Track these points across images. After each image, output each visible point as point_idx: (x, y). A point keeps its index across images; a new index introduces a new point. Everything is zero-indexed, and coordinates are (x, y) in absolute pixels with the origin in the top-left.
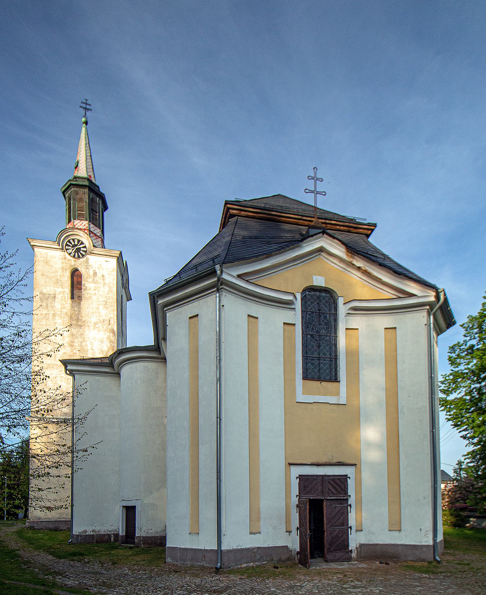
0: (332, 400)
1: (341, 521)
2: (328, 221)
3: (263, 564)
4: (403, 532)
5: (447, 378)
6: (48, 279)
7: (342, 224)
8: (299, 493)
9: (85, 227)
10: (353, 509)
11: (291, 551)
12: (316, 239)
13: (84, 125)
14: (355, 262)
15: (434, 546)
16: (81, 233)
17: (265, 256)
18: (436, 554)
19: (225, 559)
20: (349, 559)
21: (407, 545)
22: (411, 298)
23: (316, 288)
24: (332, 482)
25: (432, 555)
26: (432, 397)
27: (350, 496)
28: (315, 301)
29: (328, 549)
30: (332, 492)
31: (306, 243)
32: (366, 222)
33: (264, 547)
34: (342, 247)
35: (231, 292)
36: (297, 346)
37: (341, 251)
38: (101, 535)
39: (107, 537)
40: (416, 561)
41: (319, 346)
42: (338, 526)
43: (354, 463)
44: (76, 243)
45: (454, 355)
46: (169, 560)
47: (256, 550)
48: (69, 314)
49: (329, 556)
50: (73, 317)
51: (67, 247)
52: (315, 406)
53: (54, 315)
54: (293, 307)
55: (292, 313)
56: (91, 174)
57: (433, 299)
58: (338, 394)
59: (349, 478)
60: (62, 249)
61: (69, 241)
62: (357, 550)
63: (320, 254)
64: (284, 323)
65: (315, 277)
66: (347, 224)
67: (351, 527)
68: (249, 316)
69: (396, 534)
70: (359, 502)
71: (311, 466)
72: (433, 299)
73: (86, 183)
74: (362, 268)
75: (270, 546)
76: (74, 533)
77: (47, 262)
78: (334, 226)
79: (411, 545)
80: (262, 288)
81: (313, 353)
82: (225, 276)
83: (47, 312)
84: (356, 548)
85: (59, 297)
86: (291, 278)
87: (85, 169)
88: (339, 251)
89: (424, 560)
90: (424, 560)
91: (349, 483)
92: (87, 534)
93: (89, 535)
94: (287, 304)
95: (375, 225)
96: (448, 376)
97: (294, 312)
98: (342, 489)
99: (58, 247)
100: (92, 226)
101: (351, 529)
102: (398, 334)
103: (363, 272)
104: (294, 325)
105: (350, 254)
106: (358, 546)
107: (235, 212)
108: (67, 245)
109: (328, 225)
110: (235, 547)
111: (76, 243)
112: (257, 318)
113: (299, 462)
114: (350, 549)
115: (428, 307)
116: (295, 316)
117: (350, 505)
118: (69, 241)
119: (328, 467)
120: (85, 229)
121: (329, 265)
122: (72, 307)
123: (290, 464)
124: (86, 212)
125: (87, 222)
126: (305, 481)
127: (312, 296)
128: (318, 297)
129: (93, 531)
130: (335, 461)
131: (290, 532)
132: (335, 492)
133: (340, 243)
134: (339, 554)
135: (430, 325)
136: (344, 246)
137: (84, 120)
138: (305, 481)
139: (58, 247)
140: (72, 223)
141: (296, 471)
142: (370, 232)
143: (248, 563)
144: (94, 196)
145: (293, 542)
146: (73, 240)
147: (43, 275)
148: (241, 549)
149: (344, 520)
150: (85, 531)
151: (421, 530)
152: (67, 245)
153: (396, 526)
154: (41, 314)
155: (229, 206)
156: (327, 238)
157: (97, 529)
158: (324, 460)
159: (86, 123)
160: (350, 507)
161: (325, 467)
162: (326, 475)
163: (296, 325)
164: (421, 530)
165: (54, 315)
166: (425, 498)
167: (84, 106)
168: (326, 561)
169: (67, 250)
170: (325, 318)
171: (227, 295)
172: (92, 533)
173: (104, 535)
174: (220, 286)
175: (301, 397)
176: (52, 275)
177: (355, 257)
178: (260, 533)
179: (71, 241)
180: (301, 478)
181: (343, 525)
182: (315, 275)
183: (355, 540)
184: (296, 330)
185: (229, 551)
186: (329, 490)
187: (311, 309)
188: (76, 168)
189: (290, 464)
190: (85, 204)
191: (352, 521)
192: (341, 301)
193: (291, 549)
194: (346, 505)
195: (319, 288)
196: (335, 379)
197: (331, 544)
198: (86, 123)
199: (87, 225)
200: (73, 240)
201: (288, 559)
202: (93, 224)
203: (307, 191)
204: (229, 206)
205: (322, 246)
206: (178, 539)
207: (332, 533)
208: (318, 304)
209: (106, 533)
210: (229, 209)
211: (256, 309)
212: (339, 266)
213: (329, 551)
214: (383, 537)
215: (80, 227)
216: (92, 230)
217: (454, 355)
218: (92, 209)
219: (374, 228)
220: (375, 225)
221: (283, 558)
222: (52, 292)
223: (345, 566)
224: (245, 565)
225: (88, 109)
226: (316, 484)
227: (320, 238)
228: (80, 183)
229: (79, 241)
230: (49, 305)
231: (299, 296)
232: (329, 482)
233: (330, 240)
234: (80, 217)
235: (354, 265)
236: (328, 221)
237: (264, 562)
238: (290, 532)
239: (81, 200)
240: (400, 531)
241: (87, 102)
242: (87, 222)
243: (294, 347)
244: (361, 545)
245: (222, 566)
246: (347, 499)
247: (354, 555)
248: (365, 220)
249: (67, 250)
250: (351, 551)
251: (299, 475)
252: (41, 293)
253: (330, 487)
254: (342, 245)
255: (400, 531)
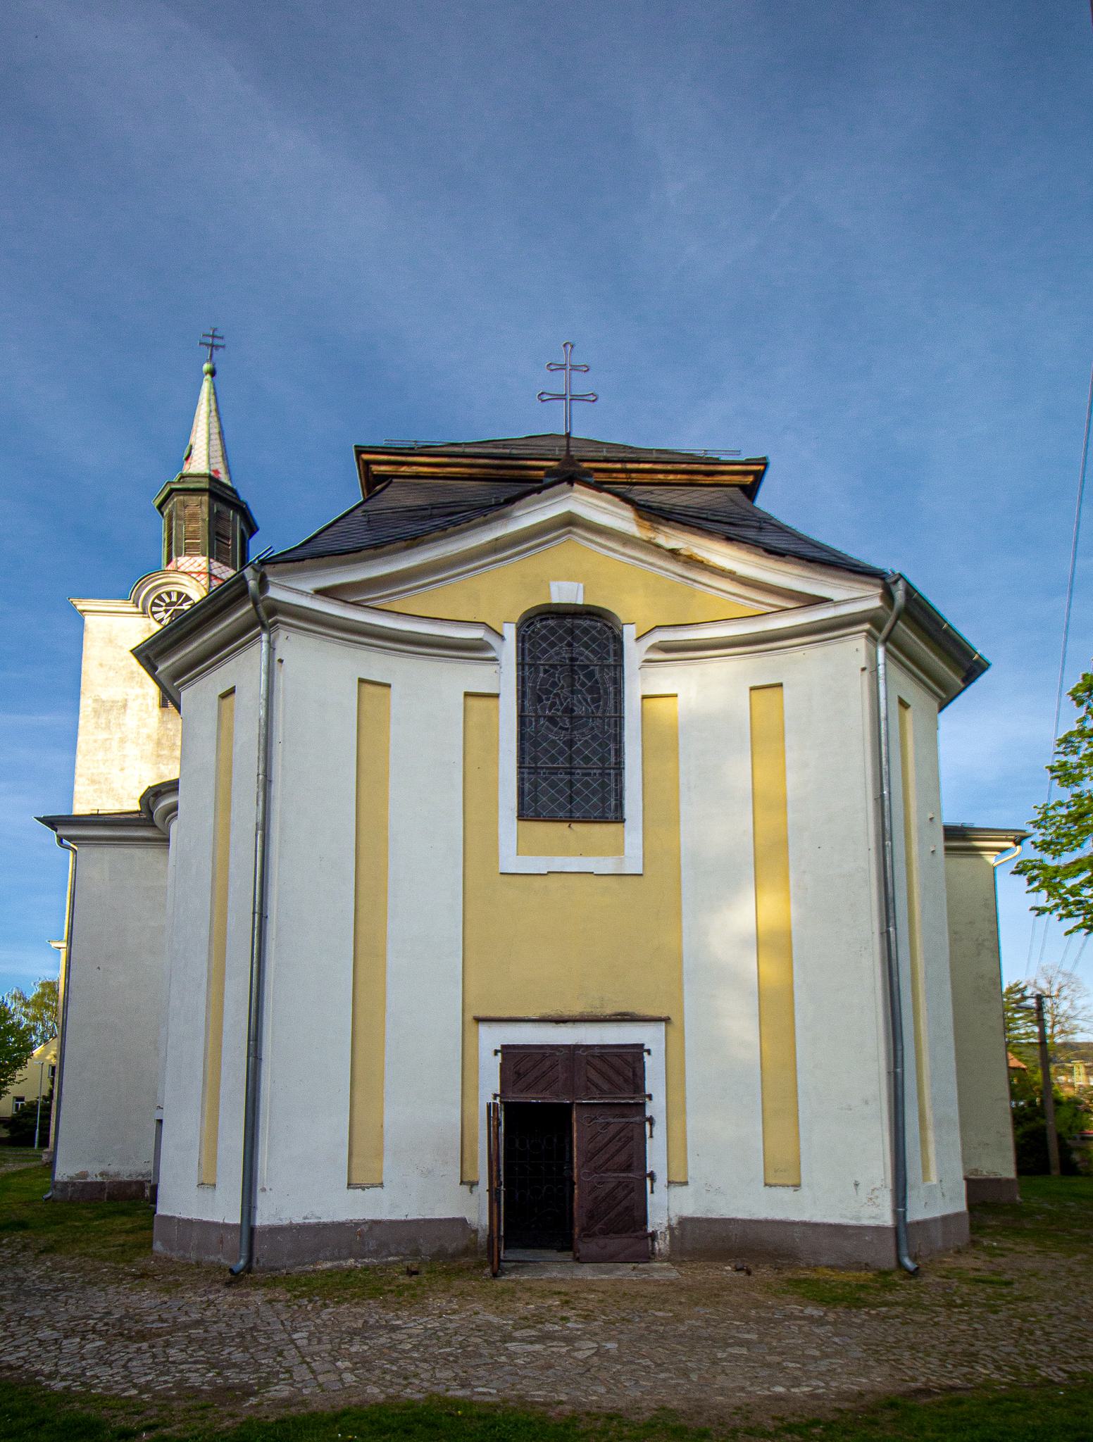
0: (605, 865)
1: (622, 1158)
2: (629, 466)
3: (388, 1264)
4: (805, 1190)
5: (1051, 813)
6: (111, 674)
7: (669, 467)
8: (502, 1091)
9: (200, 569)
10: (659, 1130)
11: (476, 1231)
12: (547, 499)
13: (208, 377)
14: (661, 540)
15: (896, 1230)
16: (184, 579)
17: (403, 544)
18: (904, 1251)
19: (261, 1248)
20: (649, 1256)
21: (816, 1225)
22: (818, 607)
23: (562, 609)
24: (597, 1062)
25: (892, 1255)
26: (884, 846)
27: (650, 1097)
28: (561, 639)
29: (583, 1230)
30: (597, 1086)
31: (520, 509)
32: (742, 459)
33: (391, 1221)
34: (623, 509)
35: (315, 632)
36: (503, 745)
37: (623, 518)
38: (120, 1183)
39: (134, 1188)
40: (842, 1268)
41: (570, 743)
42: (615, 1171)
43: (663, 1016)
44: (174, 599)
45: (1073, 759)
46: (158, 1246)
47: (365, 1228)
48: (155, 737)
49: (584, 1247)
50: (164, 741)
51: (155, 609)
52: (553, 882)
53: (123, 741)
54: (491, 655)
55: (489, 669)
56: (220, 467)
57: (876, 603)
58: (619, 850)
59: (649, 1051)
60: (144, 613)
61: (159, 597)
62: (672, 1235)
63: (570, 532)
64: (467, 695)
65: (554, 587)
66: (684, 466)
67: (652, 1175)
68: (361, 681)
69: (786, 1194)
70: (676, 1109)
71: (537, 1024)
72: (876, 603)
73: (204, 484)
74: (682, 552)
75: (409, 1218)
76: (58, 1177)
77: (111, 641)
78: (645, 476)
79: (830, 1225)
80: (394, 616)
81: (553, 759)
82: (274, 593)
83: (106, 736)
84: (670, 1228)
85: (133, 706)
86: (493, 588)
87: (205, 458)
88: (619, 518)
89: (867, 1267)
90: (867, 1267)
91: (647, 1065)
92: (89, 1180)
93: (91, 1183)
94: (473, 650)
95: (764, 463)
96: (1053, 808)
97: (496, 668)
98: (626, 1081)
99: (135, 610)
100: (216, 564)
101: (653, 1180)
102: (786, 701)
103: (685, 562)
104: (497, 696)
105: (648, 523)
106: (674, 1222)
107: (383, 468)
108: (154, 604)
109: (634, 475)
110: (298, 1220)
111: (174, 599)
112: (389, 686)
113: (506, 1015)
114: (650, 1230)
115: (867, 626)
116: (502, 676)
117: (651, 1120)
118: (159, 597)
119: (587, 1025)
120: (200, 573)
121: (591, 556)
122: (162, 722)
123: (478, 1020)
124: (202, 540)
125: (205, 558)
126: (515, 1060)
127: (552, 631)
128: (571, 632)
129: (102, 1174)
130: (609, 1010)
131: (473, 1184)
132: (606, 1087)
133: (616, 500)
134: (614, 1243)
135: (877, 670)
136: (628, 506)
137: (206, 367)
138: (515, 1060)
139: (135, 610)
140: (173, 564)
141: (493, 1038)
142: (750, 479)
143: (339, 1258)
144: (223, 508)
145: (475, 1209)
146: (169, 594)
147: (101, 665)
148: (318, 1224)
149: (631, 1156)
150: (84, 1175)
151: (856, 1185)
152: (154, 604)
153: (784, 1173)
154: (95, 741)
155: (365, 457)
156: (581, 493)
157: (113, 1169)
158: (577, 1009)
159: (213, 373)
160: (651, 1125)
161: (578, 1025)
162: (582, 1046)
163: (501, 698)
164: (856, 1185)
165: (123, 741)
166: (867, 1103)
167: (210, 340)
168: (577, 1260)
169: (154, 613)
170: (590, 675)
171: (293, 636)
172: (99, 1179)
173: (129, 1184)
174: (270, 616)
175: (510, 861)
176: (121, 664)
177: (662, 528)
178: (381, 1185)
179: (164, 596)
180: (508, 1052)
181: (628, 1168)
182: (557, 579)
183: (664, 1208)
184: (501, 707)
185: (275, 1230)
186: (589, 1080)
187: (549, 659)
188: (187, 459)
189: (478, 1020)
190: (201, 526)
191: (656, 1156)
192: (629, 633)
193: (475, 1227)
194: (637, 1119)
195: (572, 610)
196: (620, 820)
197: (592, 1216)
198: (213, 373)
199: (205, 565)
200: (169, 594)
201: (466, 1251)
202: (217, 560)
203: (545, 397)
204: (365, 457)
205: (569, 512)
206: (195, 1195)
207: (594, 1188)
208: (569, 645)
209: (134, 1178)
210: (368, 463)
211: (378, 664)
212: (623, 554)
213: (588, 1233)
214: (749, 1201)
215: (192, 569)
216: (215, 572)
217: (1073, 759)
218: (218, 534)
219: (761, 468)
220: (764, 463)
221: (451, 1247)
222: (119, 697)
223: (624, 1273)
224: (329, 1265)
225: (217, 347)
226: (552, 1067)
227: (563, 493)
228: (192, 486)
229: (180, 594)
230: (113, 721)
231: (510, 632)
232: (588, 1063)
233: (592, 496)
234: (189, 550)
235: (658, 546)
236: (629, 466)
237: (390, 1259)
238: (473, 1184)
239: (193, 517)
240: (797, 1186)
241: (217, 334)
242: (205, 558)
243: (493, 747)
244: (684, 1222)
245: (254, 1265)
246: (644, 1104)
247: (661, 1245)
248: (738, 452)
249: (154, 613)
250: (653, 1236)
251: (503, 1047)
252: (96, 701)
253: (593, 1075)
254: (622, 504)
255: (797, 1186)
